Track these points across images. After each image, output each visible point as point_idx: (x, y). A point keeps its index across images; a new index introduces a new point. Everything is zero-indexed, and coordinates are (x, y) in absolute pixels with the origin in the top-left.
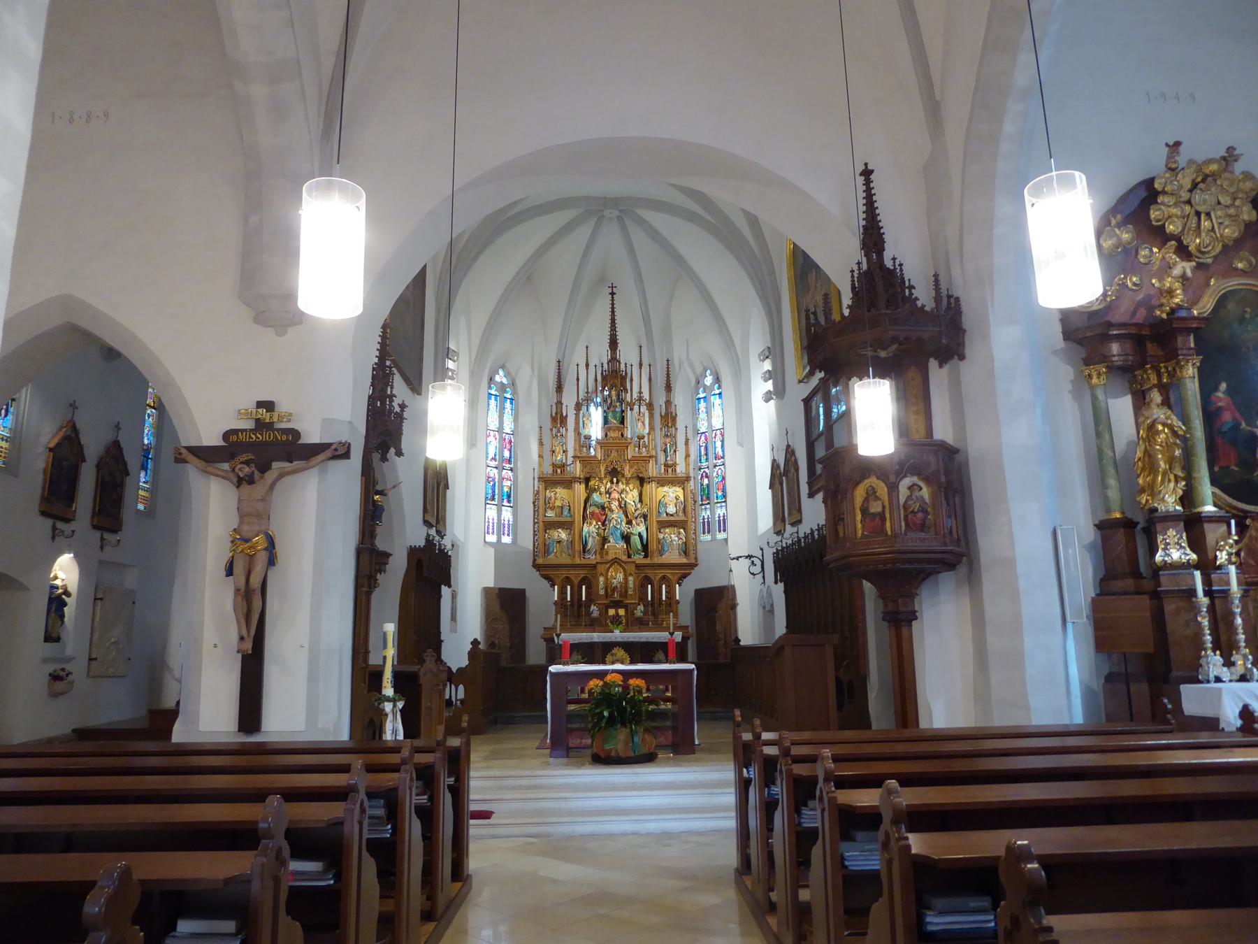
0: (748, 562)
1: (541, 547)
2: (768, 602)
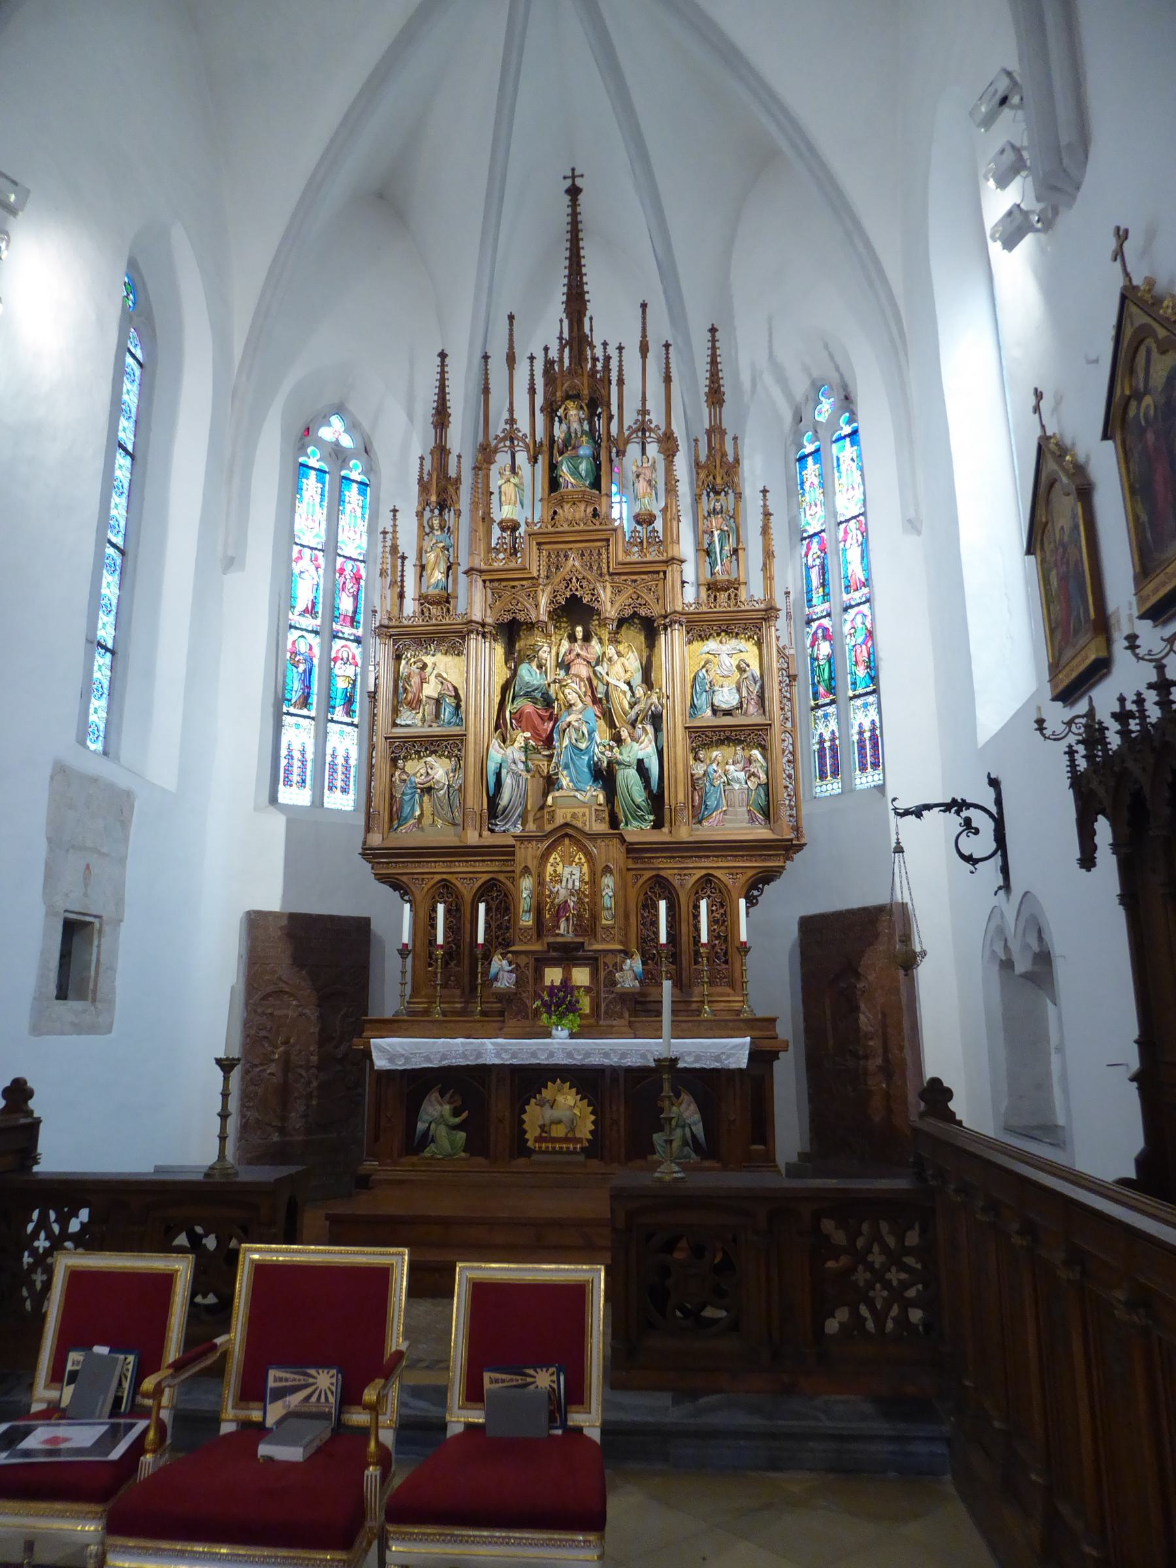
0: (953, 821)
1: (381, 804)
2: (1027, 946)
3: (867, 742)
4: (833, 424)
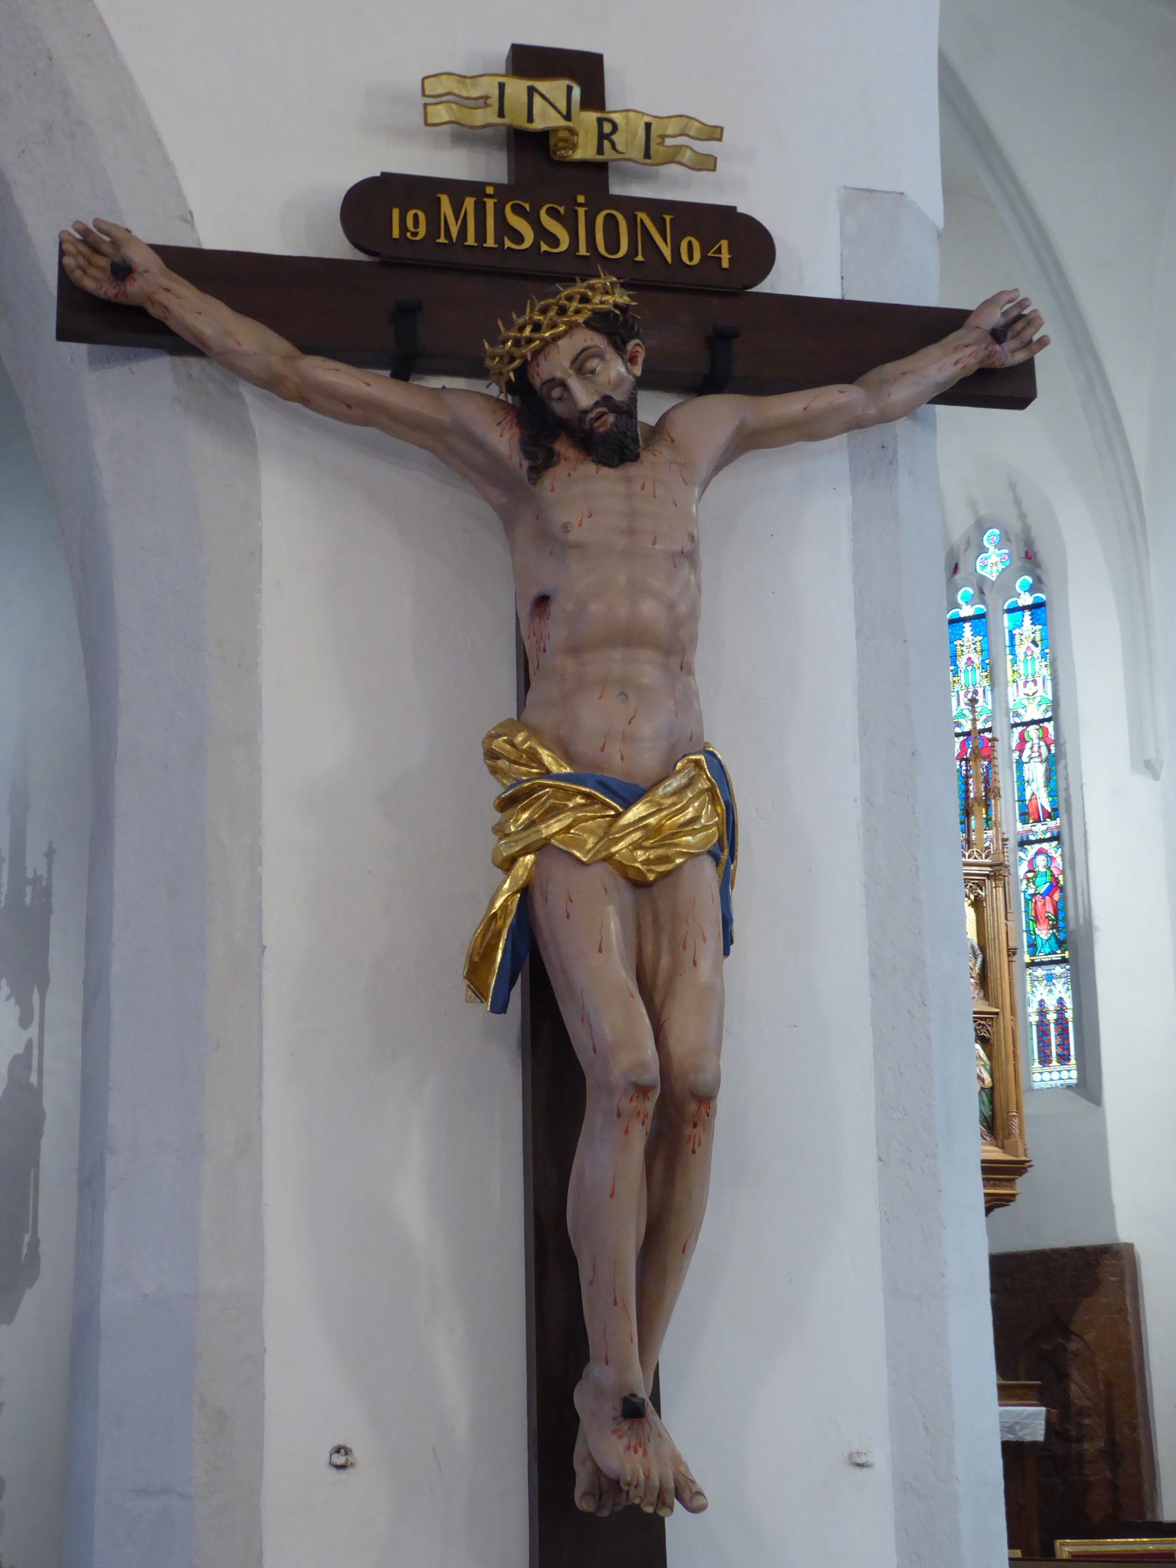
3: (1052, 1027)
4: (1005, 585)
